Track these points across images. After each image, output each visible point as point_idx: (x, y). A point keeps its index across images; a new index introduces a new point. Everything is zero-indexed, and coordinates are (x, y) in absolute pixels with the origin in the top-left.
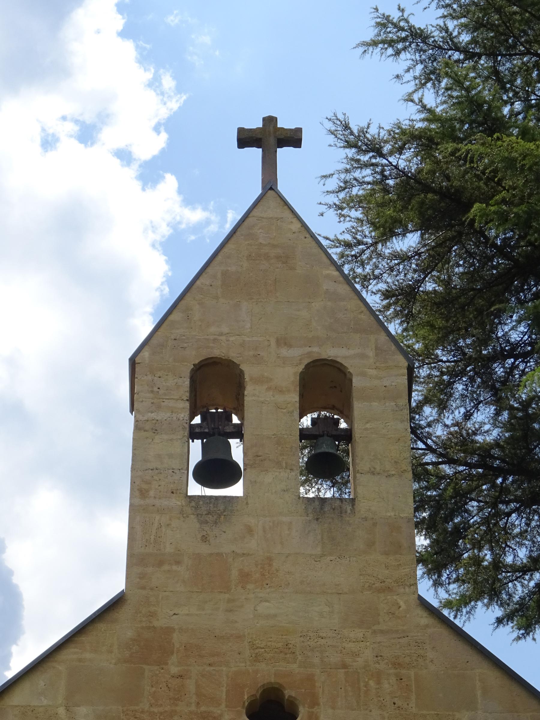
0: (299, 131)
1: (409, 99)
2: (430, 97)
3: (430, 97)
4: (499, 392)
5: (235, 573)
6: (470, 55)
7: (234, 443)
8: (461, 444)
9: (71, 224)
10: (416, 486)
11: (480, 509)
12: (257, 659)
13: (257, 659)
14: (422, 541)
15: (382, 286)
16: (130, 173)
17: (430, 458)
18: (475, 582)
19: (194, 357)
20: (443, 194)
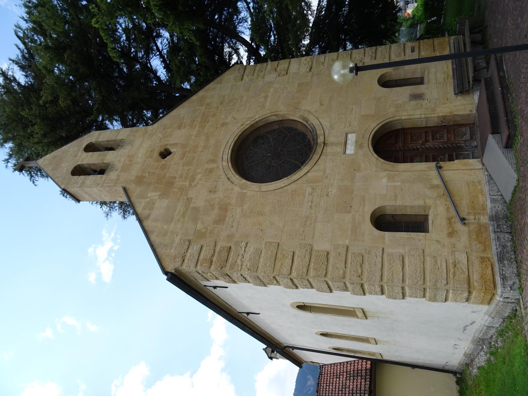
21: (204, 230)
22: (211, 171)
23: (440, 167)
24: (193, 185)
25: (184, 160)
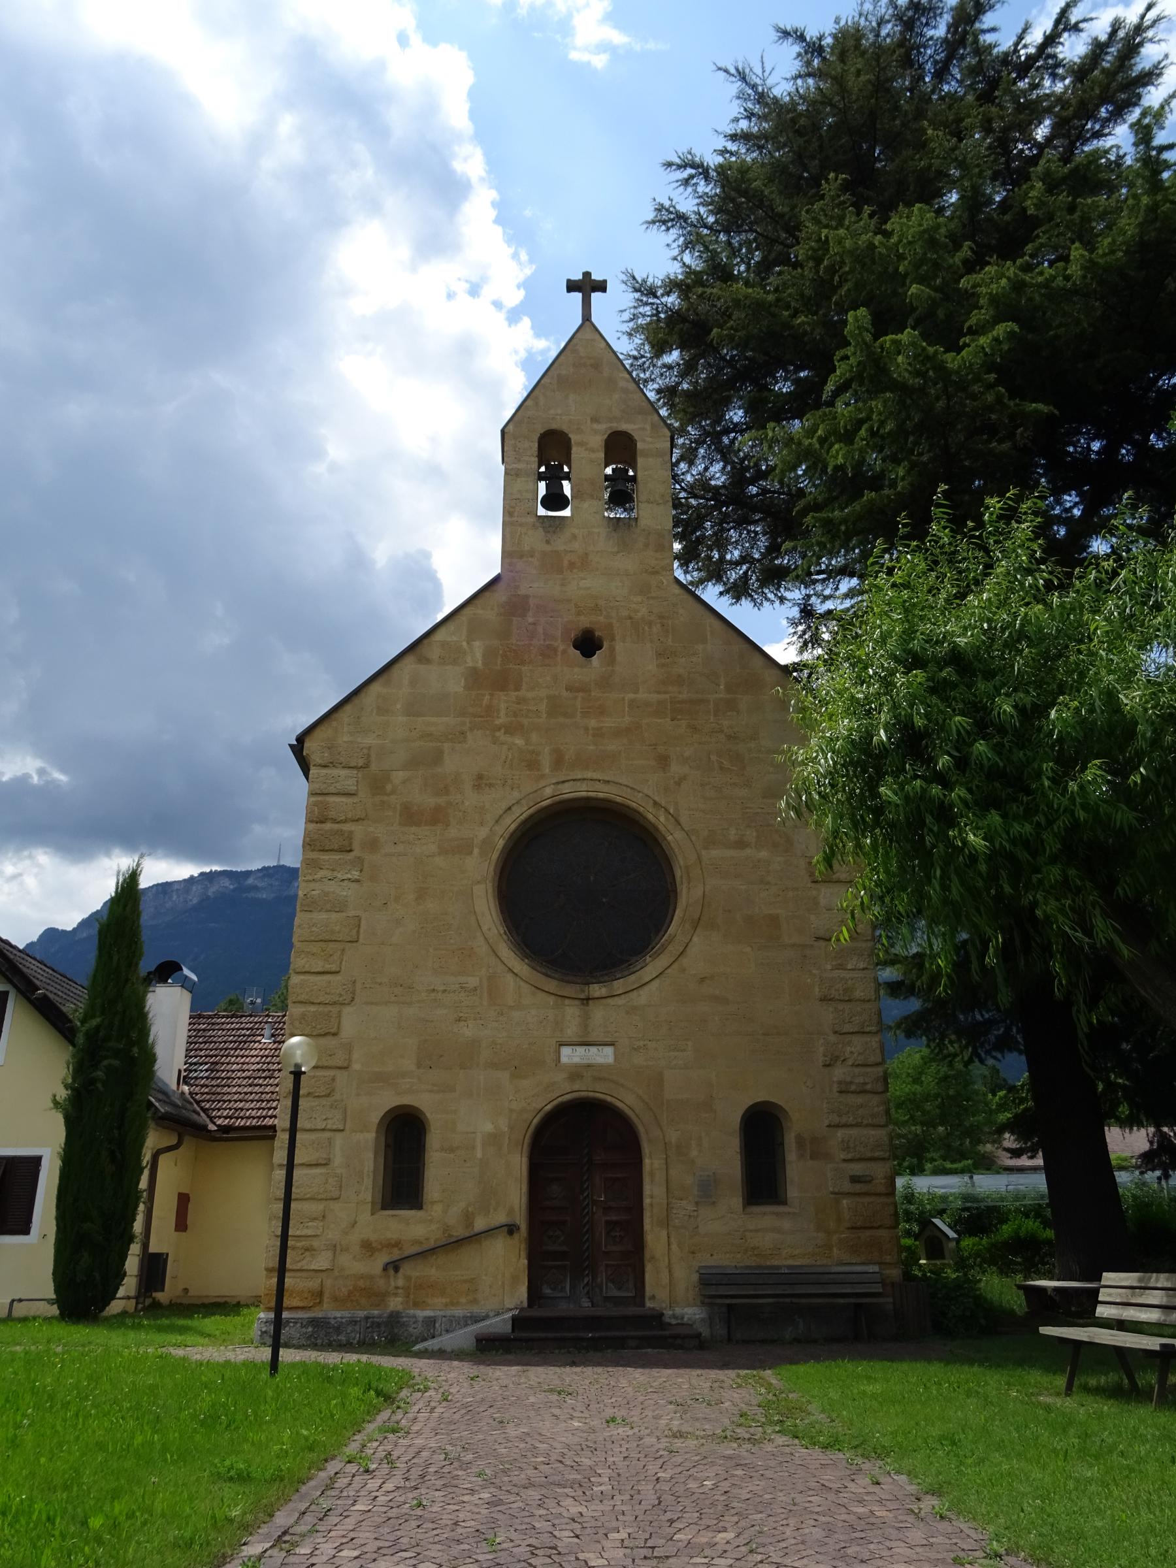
0: (605, 281)
2: (687, 258)
3: (687, 258)
4: (725, 454)
5: (566, 563)
6: (1063, 587)
7: (566, 484)
8: (702, 486)
9: (465, 350)
10: (674, 512)
11: (712, 527)
12: (579, 614)
13: (579, 614)
14: (677, 546)
15: (656, 386)
16: (501, 317)
17: (683, 495)
18: (708, 571)
19: (540, 429)
21: (389, 787)
22: (532, 764)
24: (497, 734)
25: (565, 694)
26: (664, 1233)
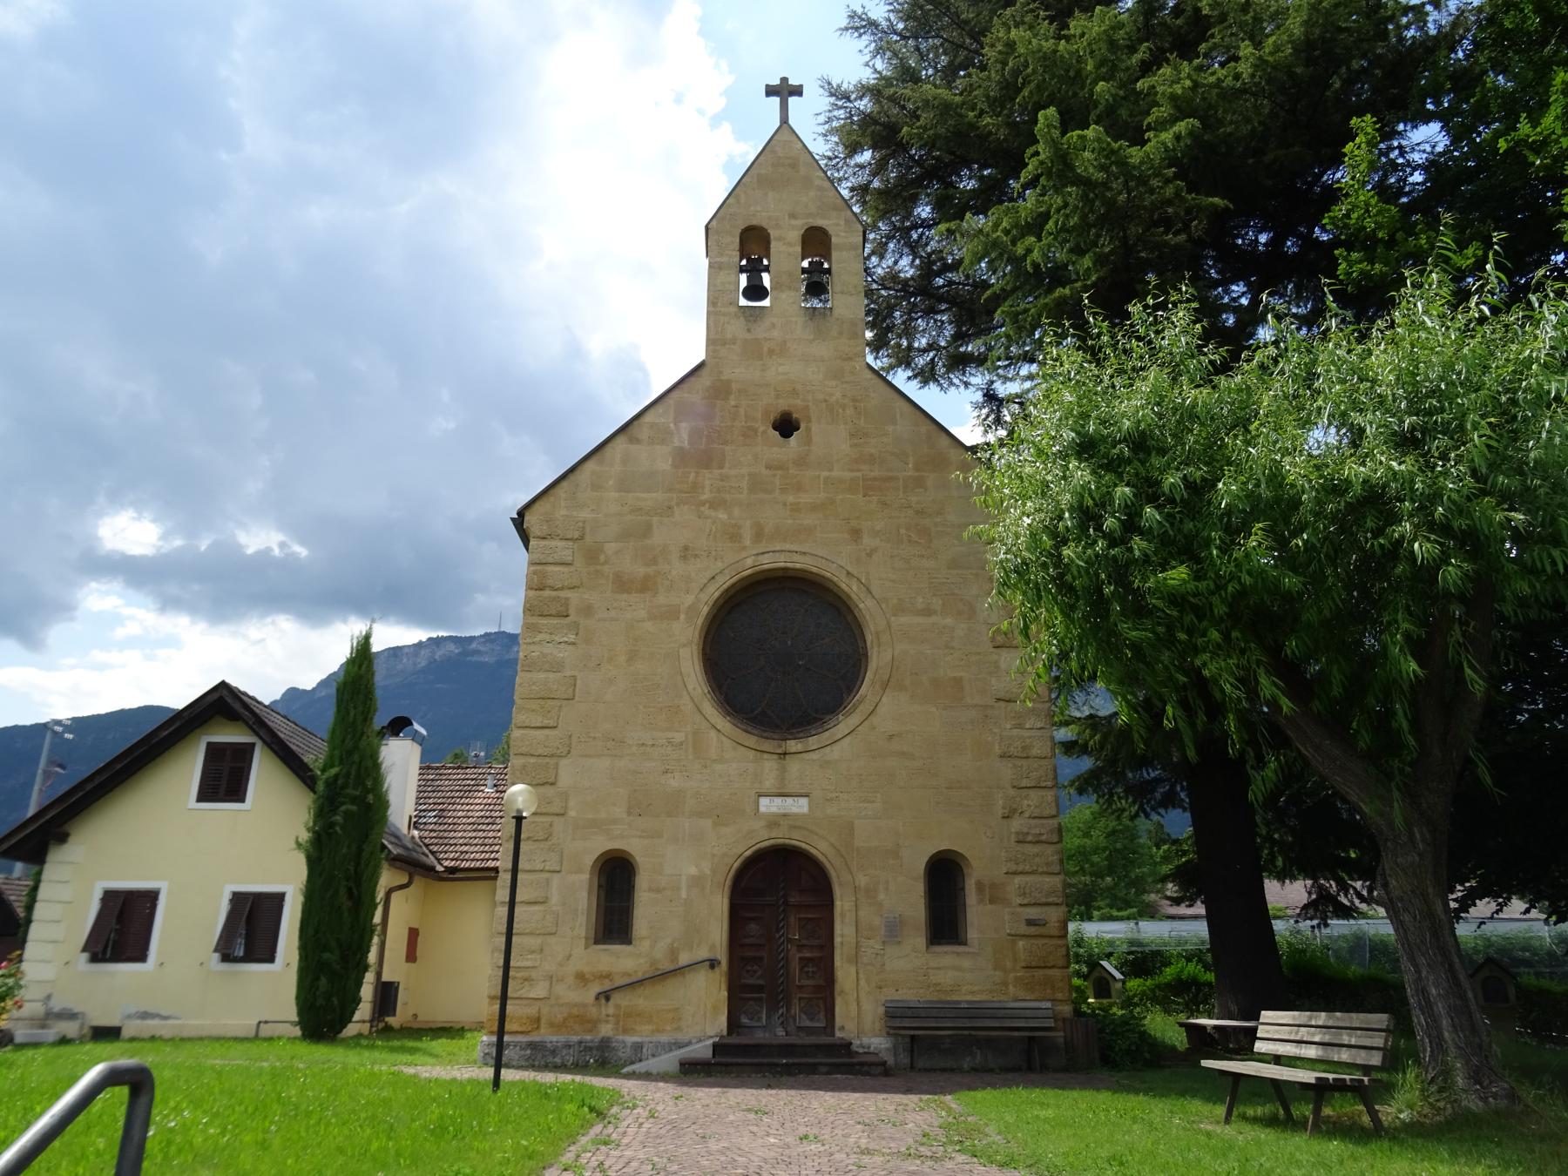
1: (867, 65)
2: (880, 64)
4: (913, 248)
6: (904, 38)
8: (893, 277)
13: (778, 397)
14: (869, 335)
17: (875, 286)
19: (698, 588)
20: (886, 126)
21: (602, 558)
23: (712, 967)
25: (765, 472)
26: (853, 970)
